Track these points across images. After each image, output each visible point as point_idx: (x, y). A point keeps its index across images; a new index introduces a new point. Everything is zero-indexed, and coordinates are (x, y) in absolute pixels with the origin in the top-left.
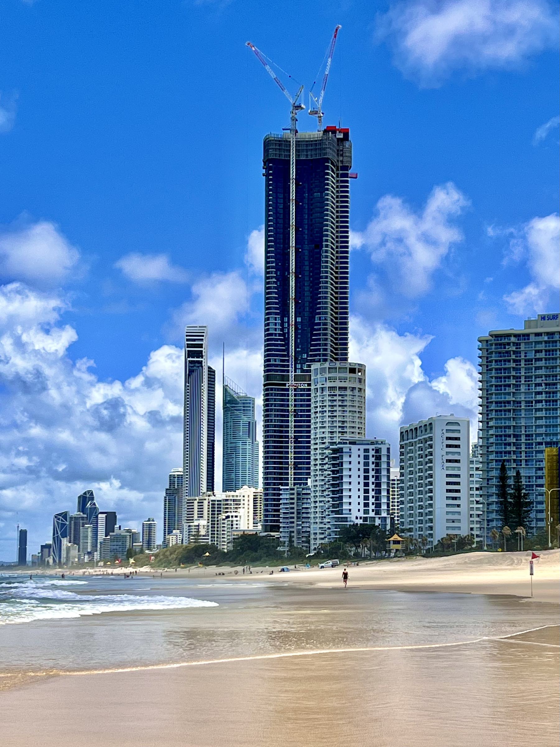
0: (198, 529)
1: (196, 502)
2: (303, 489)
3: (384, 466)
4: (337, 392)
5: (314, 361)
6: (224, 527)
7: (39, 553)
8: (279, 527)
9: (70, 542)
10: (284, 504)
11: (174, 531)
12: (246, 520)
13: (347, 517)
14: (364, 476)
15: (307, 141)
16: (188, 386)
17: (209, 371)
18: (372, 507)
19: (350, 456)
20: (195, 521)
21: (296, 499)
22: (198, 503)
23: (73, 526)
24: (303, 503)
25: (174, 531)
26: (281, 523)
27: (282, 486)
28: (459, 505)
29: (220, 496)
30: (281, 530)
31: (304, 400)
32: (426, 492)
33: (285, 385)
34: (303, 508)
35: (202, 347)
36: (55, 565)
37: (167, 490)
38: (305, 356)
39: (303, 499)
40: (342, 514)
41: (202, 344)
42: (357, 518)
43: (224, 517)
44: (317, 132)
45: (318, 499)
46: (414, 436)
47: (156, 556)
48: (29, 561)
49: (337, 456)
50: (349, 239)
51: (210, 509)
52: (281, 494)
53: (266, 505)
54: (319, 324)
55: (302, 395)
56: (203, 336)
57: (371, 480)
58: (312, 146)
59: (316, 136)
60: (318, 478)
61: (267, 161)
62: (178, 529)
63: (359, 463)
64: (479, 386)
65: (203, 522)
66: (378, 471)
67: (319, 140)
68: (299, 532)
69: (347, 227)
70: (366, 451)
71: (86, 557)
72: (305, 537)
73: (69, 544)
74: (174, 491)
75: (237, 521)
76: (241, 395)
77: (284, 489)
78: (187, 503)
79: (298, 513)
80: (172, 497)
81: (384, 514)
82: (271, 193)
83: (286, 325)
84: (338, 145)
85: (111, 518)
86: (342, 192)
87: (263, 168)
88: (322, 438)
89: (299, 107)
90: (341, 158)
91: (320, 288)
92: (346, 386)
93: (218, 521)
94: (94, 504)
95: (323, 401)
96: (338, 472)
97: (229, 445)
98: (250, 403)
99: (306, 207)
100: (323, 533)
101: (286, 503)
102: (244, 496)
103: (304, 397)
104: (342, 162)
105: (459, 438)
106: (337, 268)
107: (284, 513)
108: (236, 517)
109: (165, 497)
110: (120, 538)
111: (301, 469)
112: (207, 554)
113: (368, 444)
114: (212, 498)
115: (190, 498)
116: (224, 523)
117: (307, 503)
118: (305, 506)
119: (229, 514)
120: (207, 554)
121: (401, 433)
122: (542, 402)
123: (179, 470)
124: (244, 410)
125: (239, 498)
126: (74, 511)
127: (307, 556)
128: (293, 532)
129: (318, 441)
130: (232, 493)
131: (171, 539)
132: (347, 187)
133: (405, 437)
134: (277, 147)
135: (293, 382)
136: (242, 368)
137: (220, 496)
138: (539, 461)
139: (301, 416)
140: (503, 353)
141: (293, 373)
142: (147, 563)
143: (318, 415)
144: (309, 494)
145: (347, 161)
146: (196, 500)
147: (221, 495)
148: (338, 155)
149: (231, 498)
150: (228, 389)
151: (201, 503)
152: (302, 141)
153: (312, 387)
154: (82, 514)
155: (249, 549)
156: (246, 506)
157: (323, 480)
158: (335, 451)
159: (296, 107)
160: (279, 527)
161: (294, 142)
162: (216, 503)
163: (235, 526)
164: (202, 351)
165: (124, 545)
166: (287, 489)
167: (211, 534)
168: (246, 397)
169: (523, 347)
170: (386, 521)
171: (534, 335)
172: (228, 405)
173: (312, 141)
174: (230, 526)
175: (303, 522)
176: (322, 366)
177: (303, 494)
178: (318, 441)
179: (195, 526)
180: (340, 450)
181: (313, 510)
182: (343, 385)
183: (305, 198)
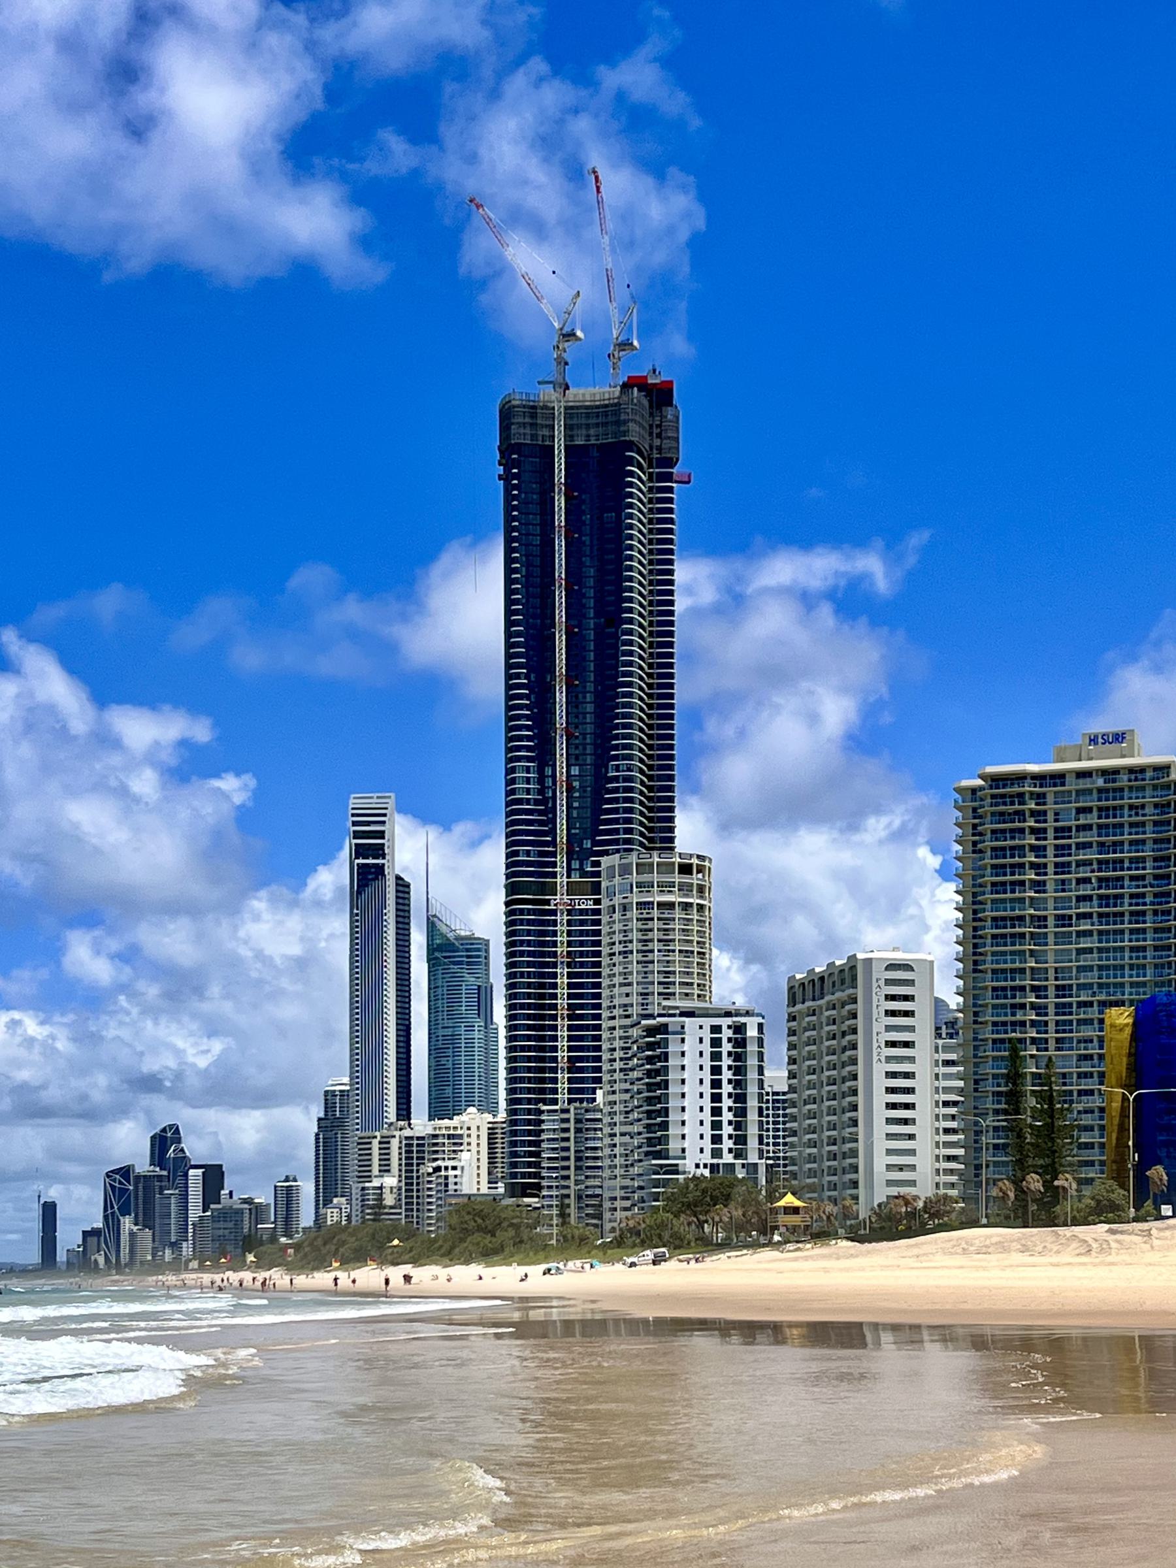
0: (381, 1194)
1: (375, 1143)
2: (587, 1111)
3: (752, 1062)
5: (606, 853)
6: (429, 1189)
7: (79, 1246)
8: (539, 1187)
9: (136, 1224)
10: (548, 1140)
11: (335, 1200)
12: (471, 1173)
13: (677, 1165)
14: (713, 1135)
15: (587, 407)
16: (357, 915)
17: (397, 885)
18: (727, 1144)
19: (683, 1040)
20: (375, 1180)
21: (572, 1130)
22: (380, 1143)
23: (140, 1193)
24: (587, 1139)
25: (335, 1200)
26: (543, 1178)
27: (545, 1104)
28: (912, 1136)
29: (421, 1128)
30: (545, 1193)
31: (587, 933)
32: (844, 1169)
33: (548, 902)
34: (587, 1148)
35: (383, 838)
36: (109, 1268)
37: (319, 1119)
38: (587, 844)
39: (587, 1129)
40: (667, 1158)
41: (383, 832)
42: (697, 1166)
43: (431, 1170)
44: (608, 389)
45: (617, 1130)
46: (817, 993)
47: (297, 1247)
48: (62, 1262)
49: (655, 1047)
50: (675, 608)
51: (404, 1162)
52: (543, 1121)
53: (514, 1144)
54: (616, 779)
55: (582, 923)
56: (385, 815)
57: (727, 1089)
58: (598, 417)
59: (607, 396)
60: (616, 1087)
61: (507, 449)
62: (342, 1196)
63: (701, 1068)
64: (958, 936)
65: (390, 1181)
66: (739, 1070)
67: (612, 405)
68: (579, 1198)
69: (671, 552)
70: (716, 1029)
71: (168, 1252)
72: (593, 1205)
73: (135, 1228)
74: (331, 1127)
75: (456, 1176)
76: (463, 933)
77: (549, 1111)
78: (359, 1144)
79: (578, 1159)
80: (330, 1134)
81: (753, 1158)
82: (515, 513)
83: (549, 782)
84: (651, 414)
85: (214, 1176)
86: (661, 511)
87: (500, 464)
88: (625, 1005)
89: (571, 335)
90: (657, 442)
91: (617, 696)
93: (418, 1177)
94: (182, 1150)
95: (625, 931)
96: (657, 1072)
97: (441, 1032)
98: (479, 950)
99: (588, 543)
100: (628, 1198)
101: (553, 1139)
102: (469, 1129)
103: (587, 927)
104: (659, 449)
105: (915, 1150)
106: (650, 666)
107: (549, 1159)
108: (454, 1168)
109: (317, 1135)
110: (231, 1216)
111: (581, 1017)
112: (396, 1242)
113: (719, 1016)
114: (408, 1132)
115: (363, 1134)
116: (430, 1182)
117: (594, 1139)
118: (591, 1144)
119: (439, 1163)
120: (396, 1242)
121: (791, 988)
122: (1091, 864)
123: (342, 1081)
124: (468, 963)
125: (459, 1132)
126: (143, 1166)
127: (599, 1242)
128: (568, 1196)
129: (616, 1012)
130: (446, 1122)
131: (329, 1215)
132: (671, 501)
133: (799, 997)
134: (527, 420)
135: (565, 897)
136: (460, 878)
137: (421, 1128)
138: (1085, 1041)
139: (582, 965)
140: (1010, 814)
141: (565, 880)
142: (280, 1260)
143: (616, 959)
144: (600, 1120)
145: (670, 448)
147: (425, 1126)
148: (651, 434)
149: (444, 1132)
150: (438, 923)
151: (385, 1142)
152: (578, 408)
153: (605, 903)
154: (158, 1169)
155: (478, 1231)
156: (474, 1147)
157: (627, 1091)
158: (651, 1031)
159: (564, 336)
160: (539, 1187)
161: (562, 410)
162: (415, 1142)
163: (451, 1187)
164: (383, 845)
165: (238, 1224)
166: (556, 1111)
167: (406, 1204)
168: (471, 939)
169: (1050, 807)
170: (756, 1172)
171: (1074, 775)
172: (437, 954)
173: (597, 407)
174: (443, 1188)
175: (587, 1177)
176: (623, 861)
177: (587, 1120)
178: (616, 1012)
179: (375, 1188)
180: (663, 1029)
181: (607, 1162)
183: (584, 523)
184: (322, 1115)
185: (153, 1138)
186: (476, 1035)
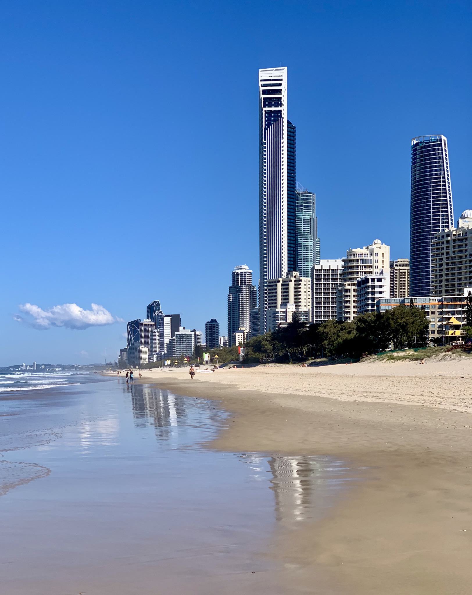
22: (282, 285)
94: (161, 312)
102: (377, 255)
124: (305, 206)
131: (237, 336)
184: (231, 285)
185: (148, 307)
186: (309, 244)
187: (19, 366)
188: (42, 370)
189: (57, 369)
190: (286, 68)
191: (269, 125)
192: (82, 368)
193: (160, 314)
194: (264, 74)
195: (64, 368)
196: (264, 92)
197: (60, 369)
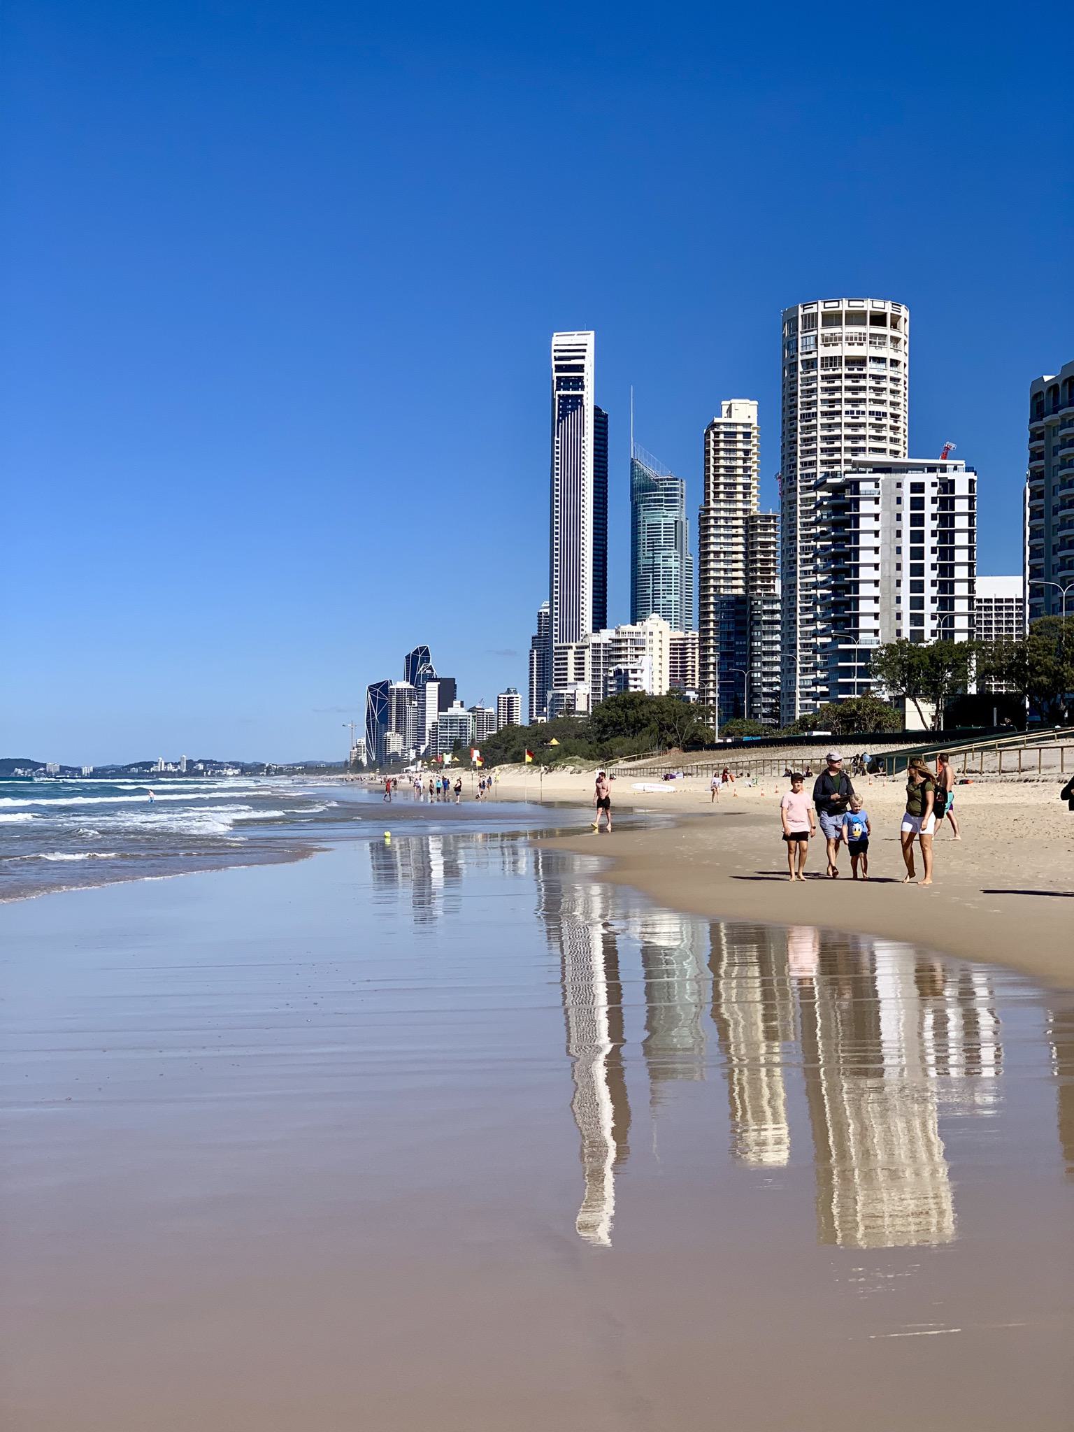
4: (844, 370)
22: (576, 653)
41: (583, 366)
70: (918, 487)
92: (864, 354)
94: (430, 668)
102: (651, 634)
121: (1036, 397)
124: (667, 501)
146: (570, 647)
156: (656, 653)
182: (856, 351)
187: (150, 764)
188: (199, 773)
189: (230, 772)
190: (592, 333)
191: (563, 415)
192: (280, 772)
193: (429, 672)
194: (560, 340)
195: (246, 770)
196: (559, 369)
197: (236, 772)
